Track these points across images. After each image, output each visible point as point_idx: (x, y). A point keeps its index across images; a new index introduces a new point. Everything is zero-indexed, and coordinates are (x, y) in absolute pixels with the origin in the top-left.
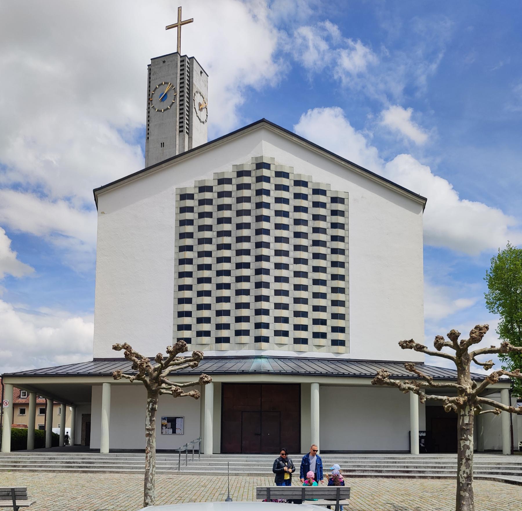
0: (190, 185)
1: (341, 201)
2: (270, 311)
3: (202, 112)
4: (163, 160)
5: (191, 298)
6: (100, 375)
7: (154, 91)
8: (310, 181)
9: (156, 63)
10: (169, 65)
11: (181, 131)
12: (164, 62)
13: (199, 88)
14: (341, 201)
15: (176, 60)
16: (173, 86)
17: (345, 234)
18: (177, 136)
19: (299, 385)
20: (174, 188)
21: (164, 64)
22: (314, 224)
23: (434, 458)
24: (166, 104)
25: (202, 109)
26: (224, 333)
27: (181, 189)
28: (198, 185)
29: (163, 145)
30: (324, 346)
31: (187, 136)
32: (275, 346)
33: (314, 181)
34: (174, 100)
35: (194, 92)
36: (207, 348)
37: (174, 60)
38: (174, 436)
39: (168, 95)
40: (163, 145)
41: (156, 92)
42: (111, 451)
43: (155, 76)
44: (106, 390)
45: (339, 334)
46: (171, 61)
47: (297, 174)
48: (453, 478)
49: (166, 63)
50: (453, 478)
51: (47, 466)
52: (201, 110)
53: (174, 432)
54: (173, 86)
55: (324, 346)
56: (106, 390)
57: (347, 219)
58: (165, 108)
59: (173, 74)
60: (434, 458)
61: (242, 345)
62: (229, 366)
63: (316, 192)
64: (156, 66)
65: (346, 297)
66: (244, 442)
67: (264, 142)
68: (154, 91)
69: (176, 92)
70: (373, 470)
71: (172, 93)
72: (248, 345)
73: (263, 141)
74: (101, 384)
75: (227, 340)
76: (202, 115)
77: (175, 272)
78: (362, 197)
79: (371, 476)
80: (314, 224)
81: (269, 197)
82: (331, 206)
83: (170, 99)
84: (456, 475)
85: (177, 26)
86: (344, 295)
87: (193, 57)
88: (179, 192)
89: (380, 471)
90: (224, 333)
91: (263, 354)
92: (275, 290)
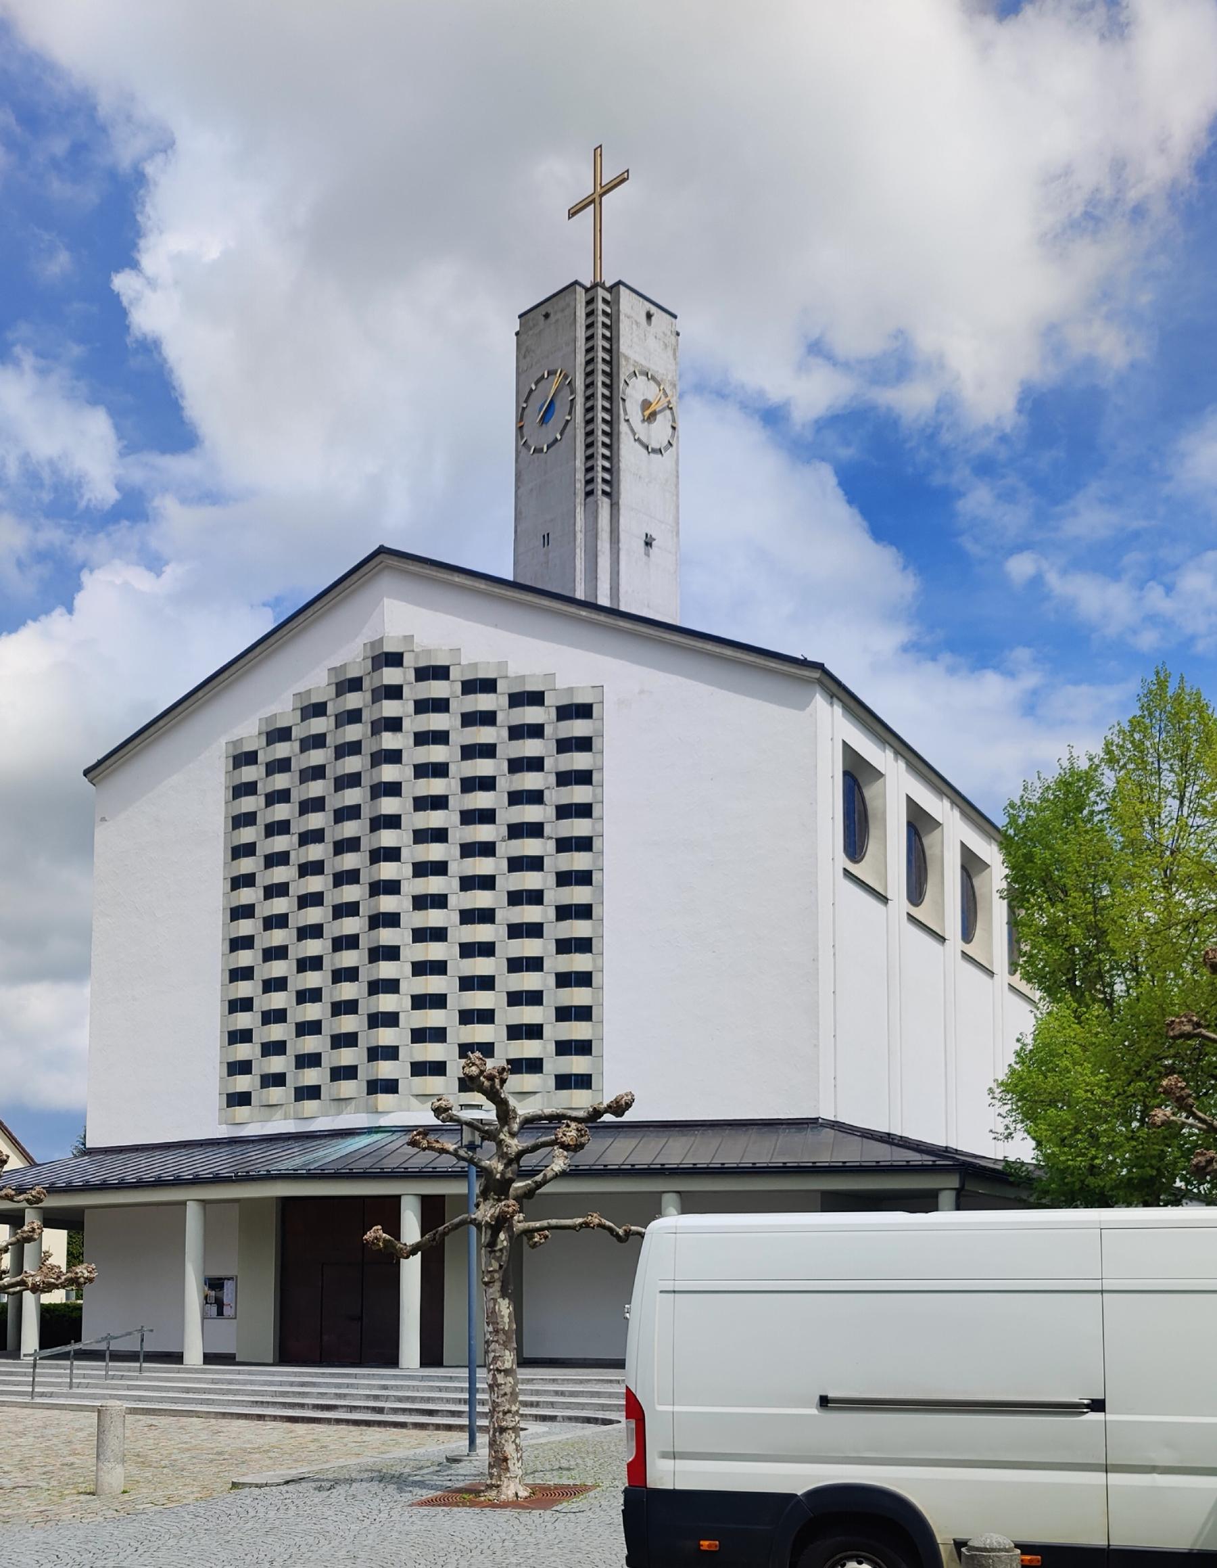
0: (248, 732)
1: (584, 711)
2: (402, 1017)
3: (654, 425)
4: (539, 586)
5: (542, 958)
6: (178, 1182)
7: (526, 401)
8: (503, 674)
9: (531, 324)
10: (557, 321)
11: (589, 494)
12: (547, 316)
13: (643, 362)
14: (584, 711)
15: (572, 304)
16: (566, 377)
17: (594, 795)
18: (580, 511)
19: (443, 1196)
20: (223, 741)
21: (549, 321)
22: (511, 782)
23: (581, 1382)
24: (552, 430)
25: (653, 415)
26: (385, 1069)
27: (235, 743)
28: (265, 729)
29: (546, 538)
30: (535, 1093)
31: (605, 503)
32: (413, 1100)
33: (511, 673)
34: (570, 414)
35: (622, 377)
36: (279, 1113)
37: (568, 305)
38: (221, 1322)
39: (557, 404)
40: (546, 538)
41: (530, 402)
42: (209, 1358)
43: (528, 359)
44: (193, 1215)
45: (574, 1058)
46: (563, 310)
47: (470, 664)
48: (460, 1428)
49: (552, 318)
50: (460, 1428)
51: (442, 1399)
52: (651, 418)
53: (220, 1313)
54: (566, 377)
55: (535, 1093)
56: (193, 1215)
57: (599, 756)
58: (551, 440)
59: (567, 344)
60: (581, 1382)
61: (343, 1103)
62: (258, 1160)
63: (518, 699)
64: (531, 333)
65: (594, 960)
66: (325, 1338)
67: (386, 601)
68: (526, 401)
69: (573, 392)
70: (368, 1408)
71: (566, 396)
72: (354, 1102)
73: (386, 601)
74: (184, 1203)
75: (391, 1087)
76: (658, 432)
77: (223, 940)
78: (642, 692)
79: (275, 1418)
80: (511, 782)
81: (399, 735)
82: (556, 729)
83: (560, 415)
84: (465, 1421)
85: (593, 201)
86: (589, 955)
87: (620, 283)
88: (232, 752)
89: (380, 1410)
90: (385, 1069)
91: (384, 1121)
92: (414, 964)
